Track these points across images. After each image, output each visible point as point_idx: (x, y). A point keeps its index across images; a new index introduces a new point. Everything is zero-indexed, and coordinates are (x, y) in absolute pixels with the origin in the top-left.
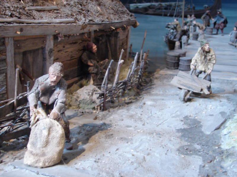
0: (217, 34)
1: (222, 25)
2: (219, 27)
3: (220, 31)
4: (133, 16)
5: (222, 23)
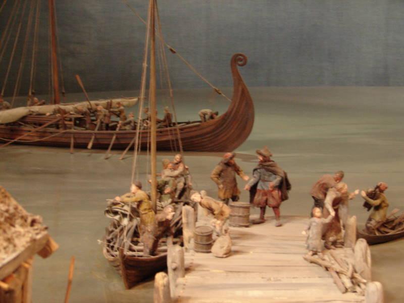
0: (261, 221)
1: (276, 193)
2: (266, 202)
3: (269, 212)
4: (40, 223)
5: (275, 188)
